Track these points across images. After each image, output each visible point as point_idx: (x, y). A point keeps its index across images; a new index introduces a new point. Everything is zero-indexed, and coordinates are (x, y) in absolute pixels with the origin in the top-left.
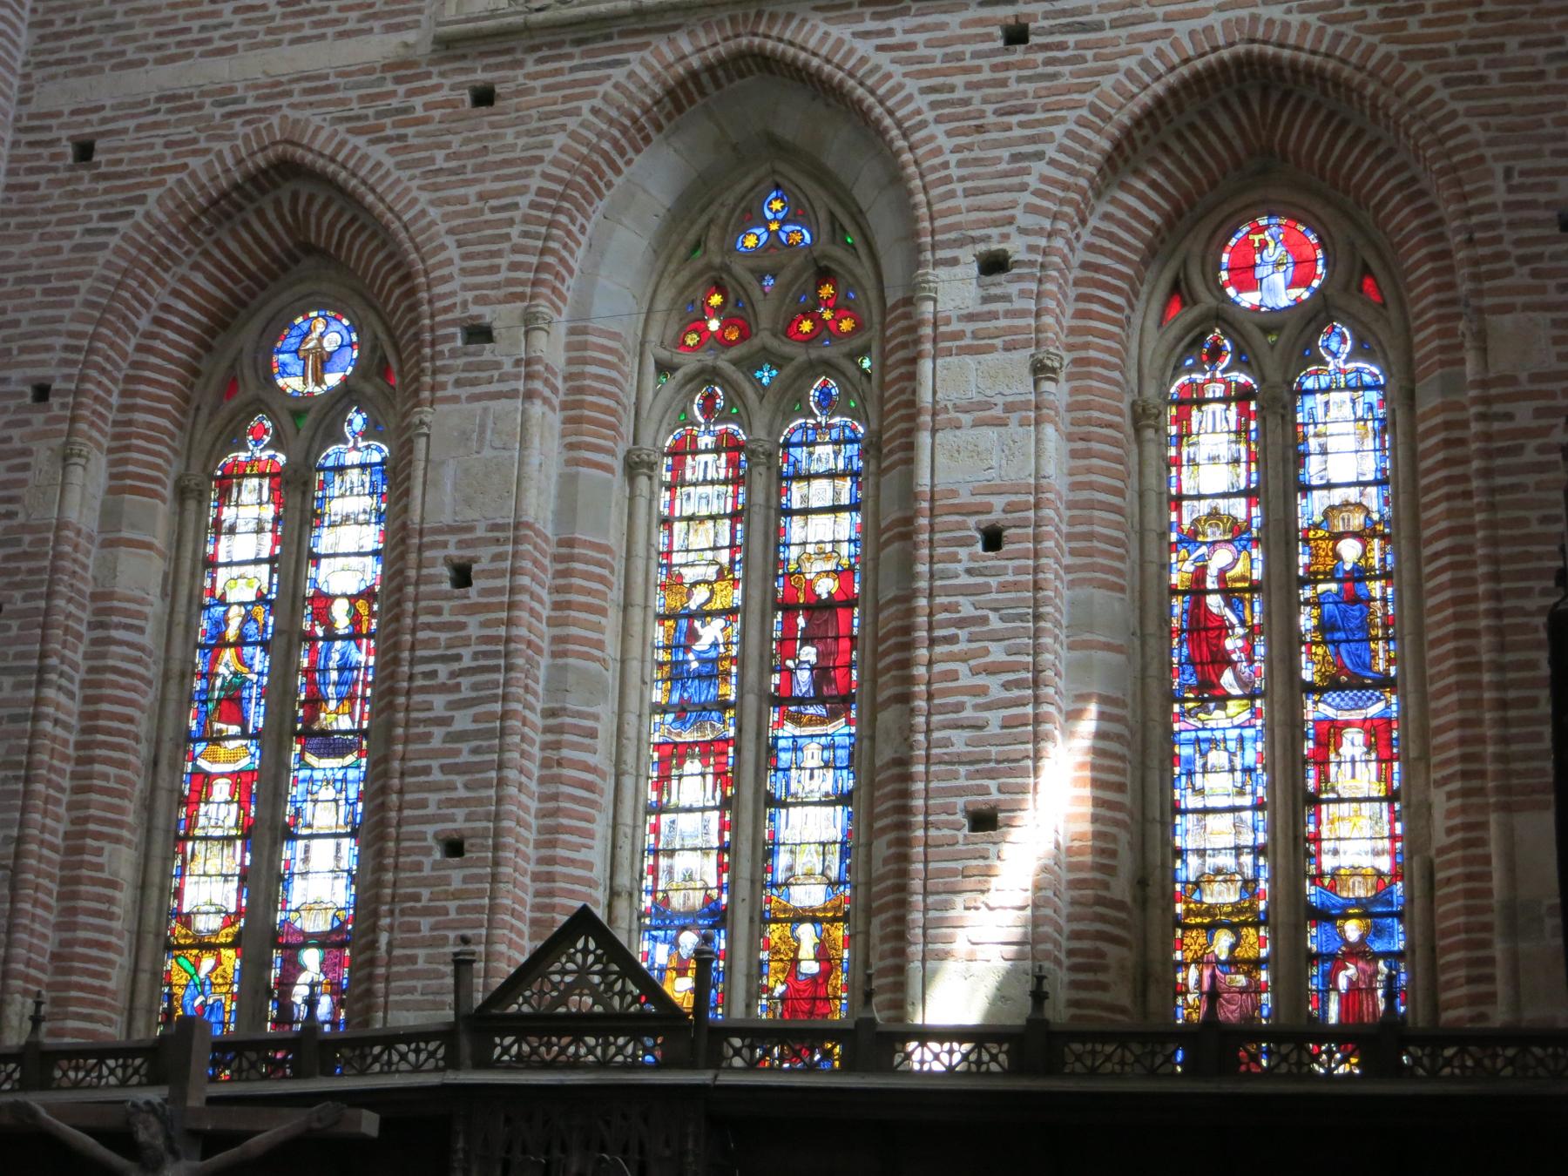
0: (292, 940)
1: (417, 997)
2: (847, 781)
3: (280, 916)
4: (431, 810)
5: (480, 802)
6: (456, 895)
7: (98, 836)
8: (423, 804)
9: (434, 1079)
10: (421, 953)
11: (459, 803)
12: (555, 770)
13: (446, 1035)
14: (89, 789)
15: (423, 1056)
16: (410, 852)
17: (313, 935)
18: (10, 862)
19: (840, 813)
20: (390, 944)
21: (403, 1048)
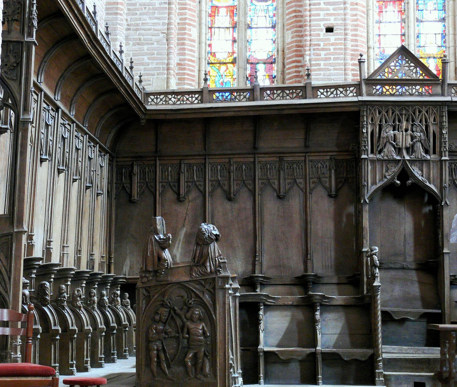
0: (253, 62)
1: (322, 77)
2: (442, 15)
3: (248, 54)
4: (322, 17)
5: (339, 14)
6: (332, 44)
7: (190, 25)
8: (318, 15)
9: (355, 99)
10: (322, 63)
11: (331, 15)
12: (355, 7)
13: (358, 86)
14: (185, 9)
15: (329, 93)
16: (315, 30)
17: (261, 60)
18: (166, 31)
19: (441, 24)
20: (310, 60)
21: (152, 97)
